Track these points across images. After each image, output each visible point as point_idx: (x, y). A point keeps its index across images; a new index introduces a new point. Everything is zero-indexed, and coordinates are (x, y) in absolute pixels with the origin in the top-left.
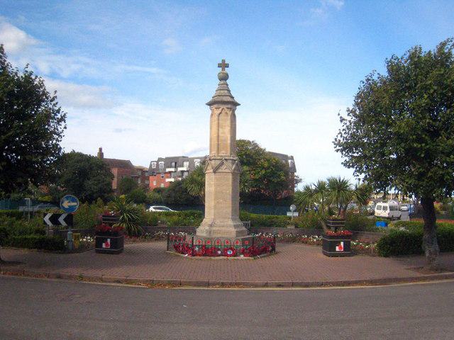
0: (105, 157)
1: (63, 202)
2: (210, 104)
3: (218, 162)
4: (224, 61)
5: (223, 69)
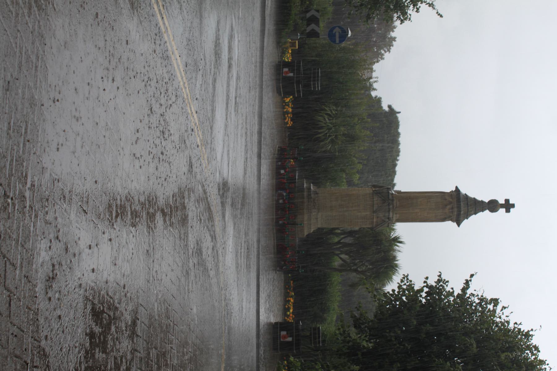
4: (513, 206)
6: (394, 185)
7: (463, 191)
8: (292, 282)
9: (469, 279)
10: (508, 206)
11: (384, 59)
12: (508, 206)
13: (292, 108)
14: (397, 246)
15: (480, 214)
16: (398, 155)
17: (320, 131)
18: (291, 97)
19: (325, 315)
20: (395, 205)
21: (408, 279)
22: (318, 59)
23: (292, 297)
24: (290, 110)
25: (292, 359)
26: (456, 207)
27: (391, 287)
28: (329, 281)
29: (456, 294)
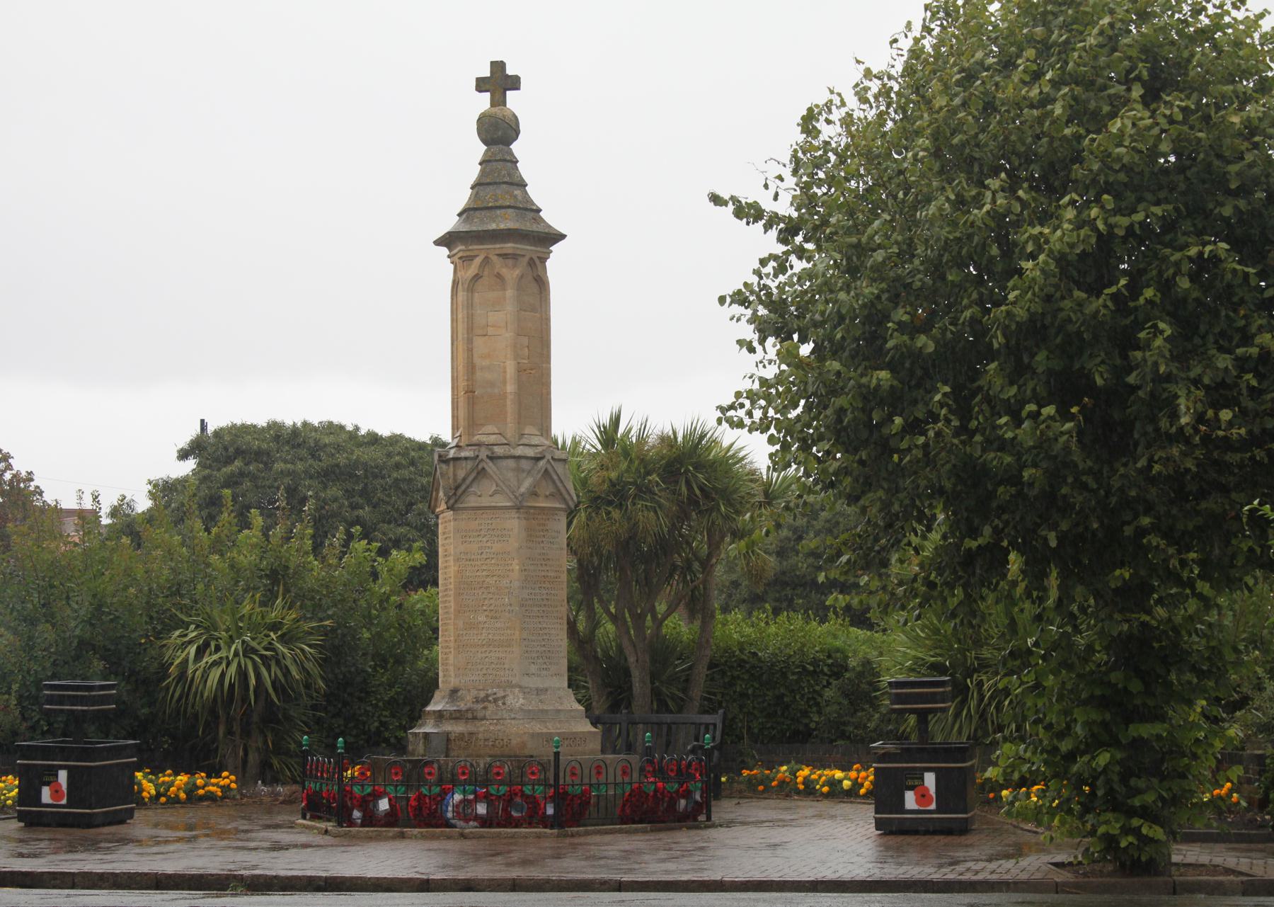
4: (498, 67)
6: (437, 442)
7: (449, 222)
8: (745, 773)
9: (731, 207)
10: (499, 82)
11: (30, 473)
12: (499, 82)
13: (177, 774)
14: (564, 443)
15: (525, 169)
16: (341, 428)
17: (253, 681)
18: (139, 775)
19: (852, 663)
20: (492, 439)
21: (732, 407)
22: (15, 687)
23: (794, 773)
24: (182, 779)
25: (991, 773)
26: (502, 240)
27: (757, 451)
28: (742, 650)
29: (780, 249)
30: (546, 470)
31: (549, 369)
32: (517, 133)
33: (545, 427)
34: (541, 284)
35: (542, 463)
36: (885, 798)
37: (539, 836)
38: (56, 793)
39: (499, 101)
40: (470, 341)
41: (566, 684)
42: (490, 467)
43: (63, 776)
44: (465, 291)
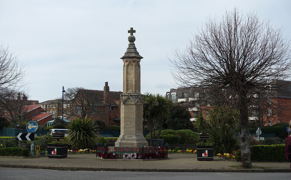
0: (110, 90)
1: (28, 126)
2: (123, 58)
3: (126, 97)
4: (132, 29)
5: (132, 34)
6: (120, 93)
7: (123, 55)
20: (131, 92)
26: (132, 58)
30: (140, 98)
31: (140, 80)
32: (135, 40)
33: (139, 91)
34: (139, 66)
35: (139, 96)
36: (199, 154)
37: (140, 161)
38: (54, 152)
39: (132, 34)
40: (127, 76)
41: (143, 134)
42: (130, 97)
43: (56, 149)
44: (127, 68)
